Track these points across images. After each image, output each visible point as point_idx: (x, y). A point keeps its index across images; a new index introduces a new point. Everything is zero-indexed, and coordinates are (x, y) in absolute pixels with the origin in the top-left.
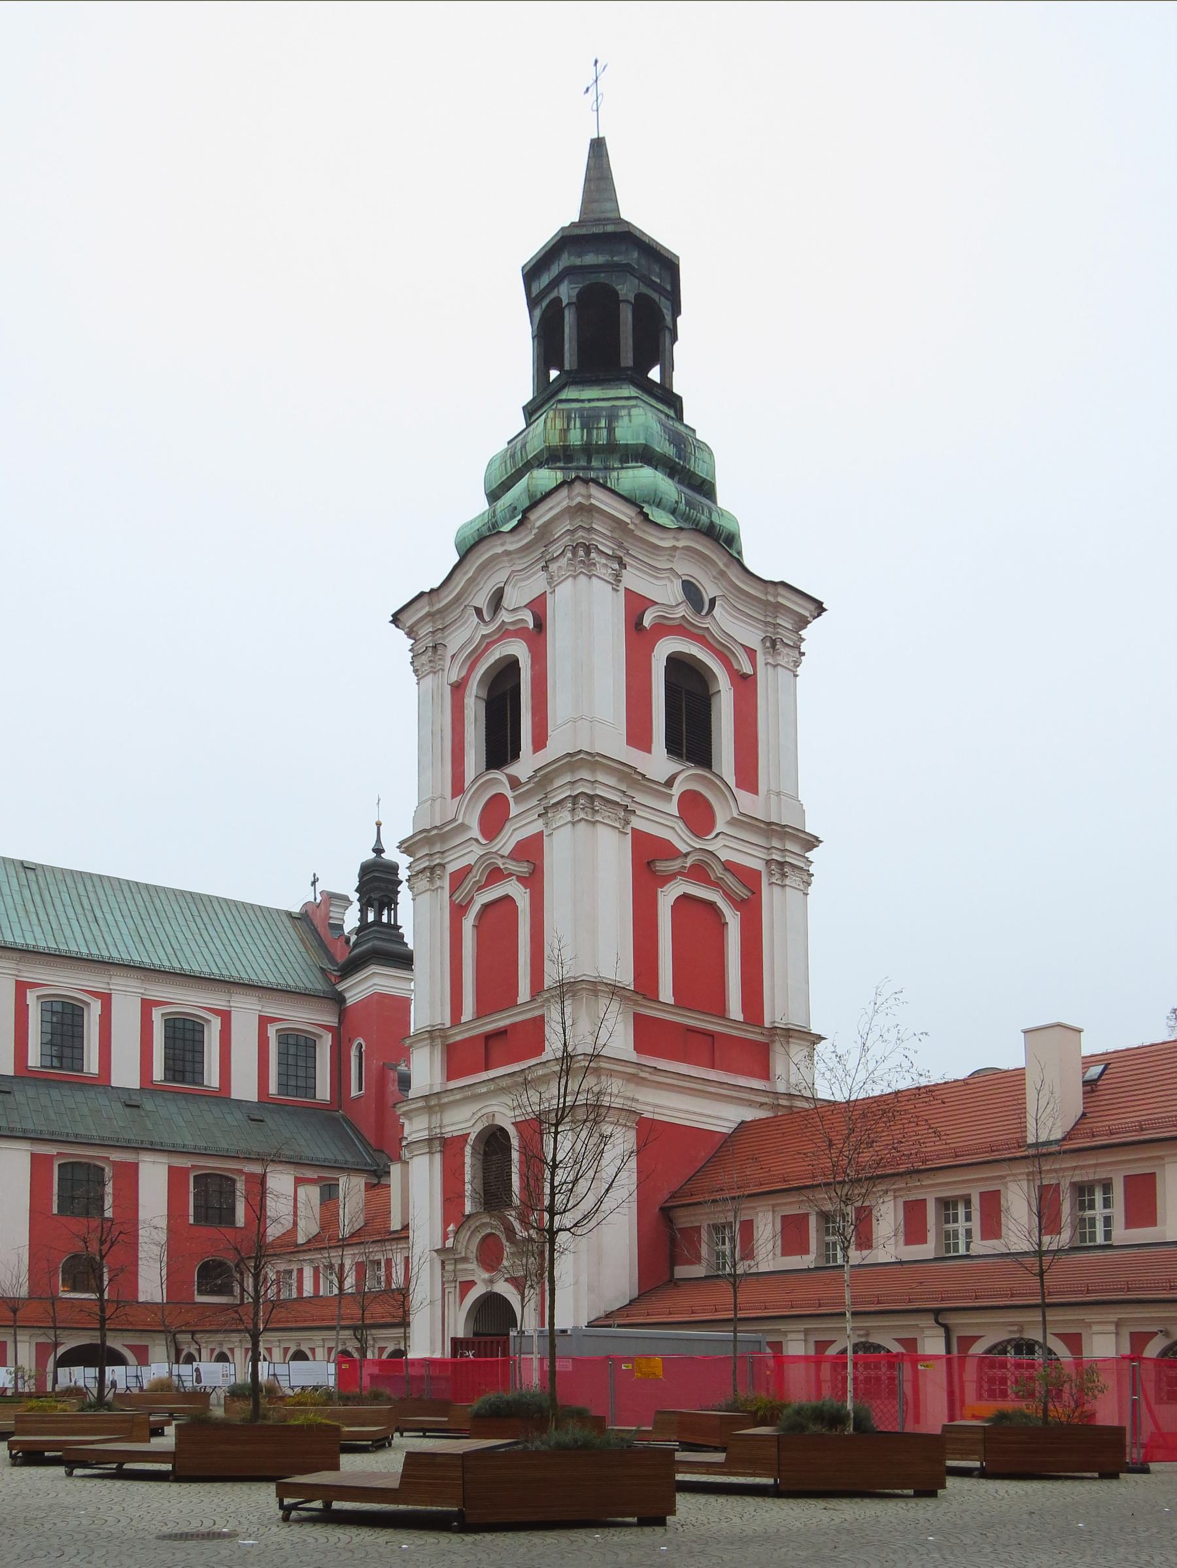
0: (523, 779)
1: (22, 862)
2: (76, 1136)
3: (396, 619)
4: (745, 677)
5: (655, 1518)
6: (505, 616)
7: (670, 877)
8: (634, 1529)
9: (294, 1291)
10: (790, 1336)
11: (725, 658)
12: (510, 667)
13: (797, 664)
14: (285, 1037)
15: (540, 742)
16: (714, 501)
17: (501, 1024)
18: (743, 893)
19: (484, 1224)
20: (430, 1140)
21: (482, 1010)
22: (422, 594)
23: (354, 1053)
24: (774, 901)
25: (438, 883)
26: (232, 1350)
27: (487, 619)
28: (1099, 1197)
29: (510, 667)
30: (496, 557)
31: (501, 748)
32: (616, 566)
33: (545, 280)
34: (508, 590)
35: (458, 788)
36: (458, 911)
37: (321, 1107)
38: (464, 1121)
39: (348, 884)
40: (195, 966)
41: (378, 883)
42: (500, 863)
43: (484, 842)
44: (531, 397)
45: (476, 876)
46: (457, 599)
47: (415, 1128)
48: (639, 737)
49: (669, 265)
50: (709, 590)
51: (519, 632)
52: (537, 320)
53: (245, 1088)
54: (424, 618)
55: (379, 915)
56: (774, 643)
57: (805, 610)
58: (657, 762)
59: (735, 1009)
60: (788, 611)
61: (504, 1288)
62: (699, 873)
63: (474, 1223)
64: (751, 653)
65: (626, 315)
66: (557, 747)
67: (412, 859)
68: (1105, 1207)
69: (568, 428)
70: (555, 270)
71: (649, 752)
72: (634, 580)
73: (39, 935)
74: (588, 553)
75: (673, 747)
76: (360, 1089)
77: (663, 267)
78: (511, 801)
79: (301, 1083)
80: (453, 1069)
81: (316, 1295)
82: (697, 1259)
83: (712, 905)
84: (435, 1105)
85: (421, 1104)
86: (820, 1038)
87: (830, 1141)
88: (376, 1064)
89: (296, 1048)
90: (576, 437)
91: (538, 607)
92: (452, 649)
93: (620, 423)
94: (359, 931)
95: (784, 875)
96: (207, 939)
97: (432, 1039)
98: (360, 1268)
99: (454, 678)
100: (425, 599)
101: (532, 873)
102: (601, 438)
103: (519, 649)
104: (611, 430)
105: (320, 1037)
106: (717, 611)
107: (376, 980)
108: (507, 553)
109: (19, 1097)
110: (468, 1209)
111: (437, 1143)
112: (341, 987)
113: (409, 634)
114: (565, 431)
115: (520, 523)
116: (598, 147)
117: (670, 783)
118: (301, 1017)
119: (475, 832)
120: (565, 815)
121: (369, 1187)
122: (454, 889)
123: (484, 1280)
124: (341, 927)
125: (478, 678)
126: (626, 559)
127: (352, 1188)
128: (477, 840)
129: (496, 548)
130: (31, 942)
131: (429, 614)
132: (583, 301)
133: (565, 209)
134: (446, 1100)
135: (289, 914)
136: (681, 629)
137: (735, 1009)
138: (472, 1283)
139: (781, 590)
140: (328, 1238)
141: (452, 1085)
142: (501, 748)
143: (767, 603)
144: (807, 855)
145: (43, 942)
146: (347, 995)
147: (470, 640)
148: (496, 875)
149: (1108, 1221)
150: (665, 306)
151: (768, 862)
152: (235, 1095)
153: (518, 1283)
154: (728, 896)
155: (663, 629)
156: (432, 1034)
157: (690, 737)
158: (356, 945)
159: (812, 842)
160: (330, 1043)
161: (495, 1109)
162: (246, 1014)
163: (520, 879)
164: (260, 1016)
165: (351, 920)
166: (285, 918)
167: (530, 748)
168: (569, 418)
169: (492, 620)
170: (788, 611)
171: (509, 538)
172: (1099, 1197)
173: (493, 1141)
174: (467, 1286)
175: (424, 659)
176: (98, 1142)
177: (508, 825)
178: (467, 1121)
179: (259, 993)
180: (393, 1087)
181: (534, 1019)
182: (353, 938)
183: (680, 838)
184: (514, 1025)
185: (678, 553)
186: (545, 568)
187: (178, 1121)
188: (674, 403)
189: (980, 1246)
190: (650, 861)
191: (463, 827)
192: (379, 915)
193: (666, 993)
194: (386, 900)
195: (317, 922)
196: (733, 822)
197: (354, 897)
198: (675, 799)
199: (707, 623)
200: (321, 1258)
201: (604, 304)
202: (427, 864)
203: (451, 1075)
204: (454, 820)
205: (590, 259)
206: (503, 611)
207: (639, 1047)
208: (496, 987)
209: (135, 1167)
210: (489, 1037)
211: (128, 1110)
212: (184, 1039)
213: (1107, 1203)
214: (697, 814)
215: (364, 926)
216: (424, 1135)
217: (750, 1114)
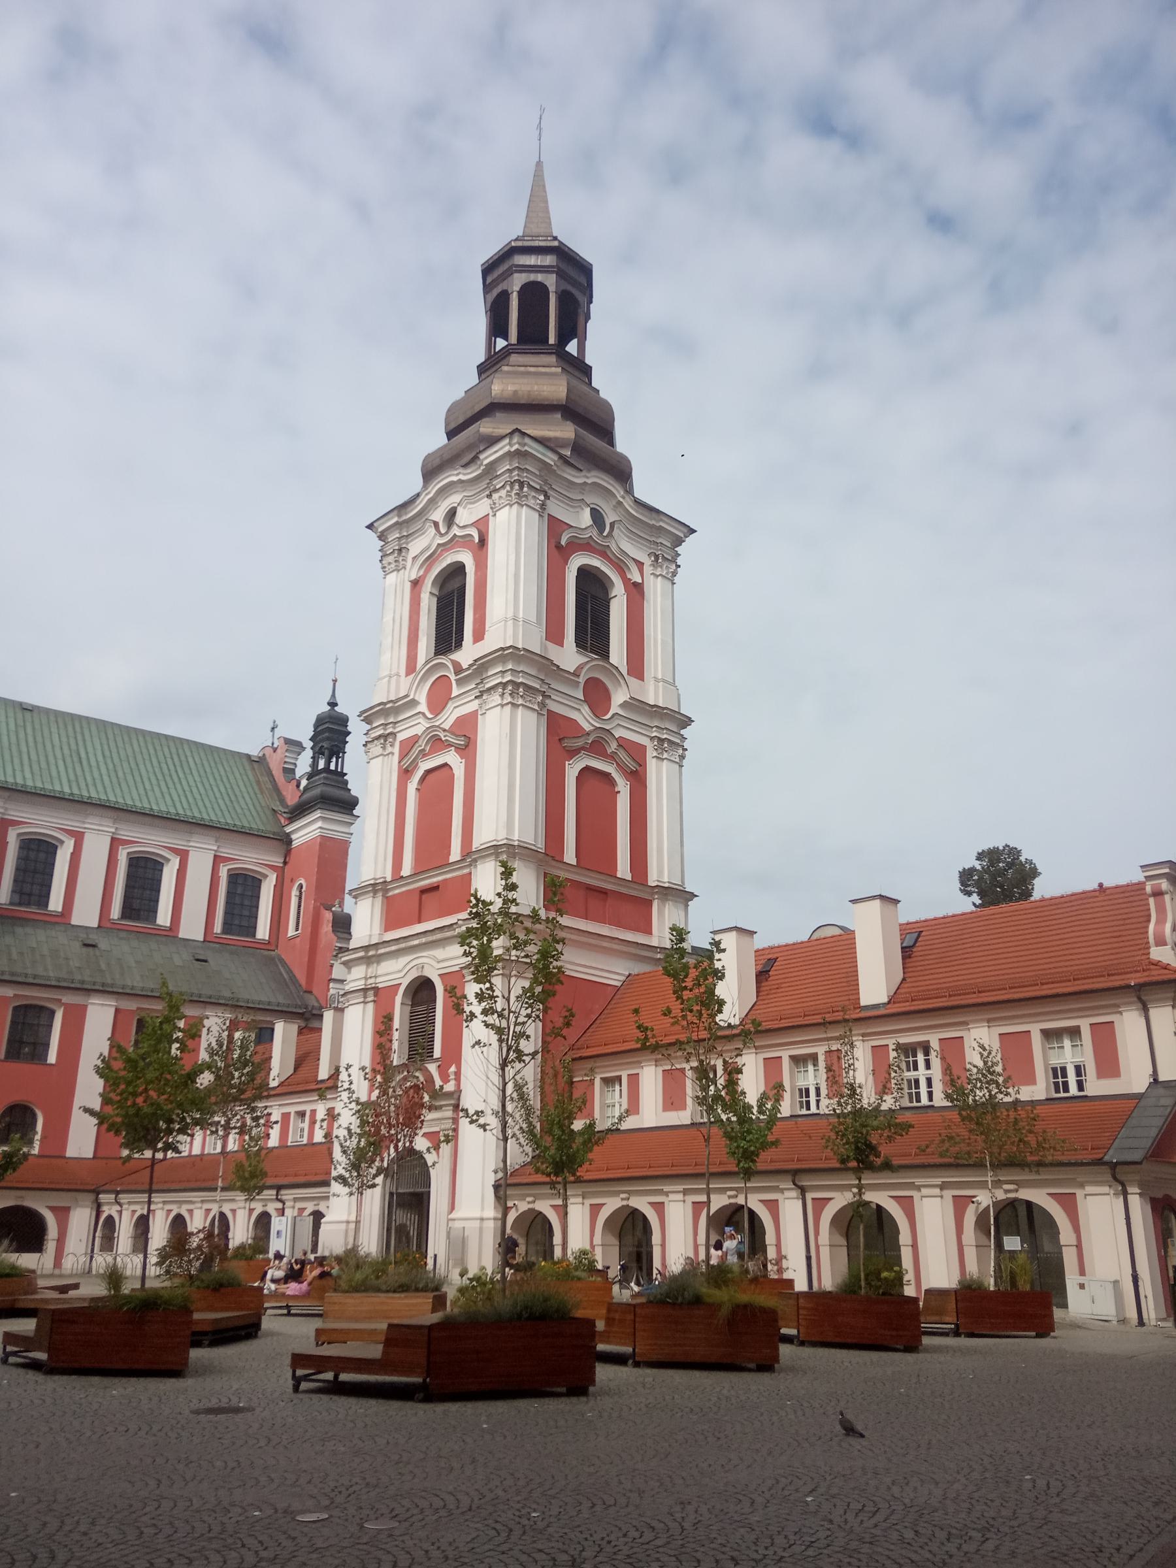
0: (465, 666)
1: (21, 704)
2: (35, 977)
4: (635, 584)
5: (580, 1387)
6: (455, 531)
8: (563, 1399)
10: (672, 1197)
11: (621, 569)
12: (458, 570)
14: (234, 877)
15: (479, 636)
16: (611, 443)
17: (435, 880)
18: (632, 766)
20: (365, 990)
23: (295, 892)
24: (658, 773)
25: (389, 749)
27: (443, 531)
29: (458, 570)
30: (452, 483)
31: (448, 636)
32: (542, 498)
34: (460, 510)
35: (411, 668)
36: (406, 773)
38: (396, 972)
39: (304, 733)
40: (160, 806)
41: (331, 733)
42: (442, 735)
43: (430, 716)
44: (483, 360)
45: (422, 743)
48: (554, 634)
49: (585, 270)
50: (610, 517)
52: (489, 305)
54: (395, 528)
55: (328, 763)
56: (657, 557)
58: (569, 656)
60: (666, 535)
64: (640, 565)
66: (494, 639)
67: (369, 727)
71: (562, 646)
72: (557, 509)
73: (28, 775)
74: (521, 487)
75: (581, 643)
76: (297, 929)
78: (454, 683)
79: (245, 923)
80: (390, 922)
83: (607, 775)
84: (373, 956)
86: (693, 896)
91: (482, 525)
92: (412, 554)
94: (310, 776)
99: (413, 577)
101: (467, 746)
106: (616, 532)
108: (461, 481)
111: (371, 993)
112: (288, 830)
117: (576, 674)
118: (250, 858)
119: (423, 707)
120: (495, 699)
121: (301, 1032)
124: (293, 771)
125: (433, 577)
126: (550, 492)
128: (424, 714)
130: (20, 781)
131: (397, 523)
135: (248, 756)
136: (587, 546)
142: (448, 636)
144: (682, 732)
146: (293, 837)
147: (427, 548)
148: (437, 743)
152: (182, 934)
154: (621, 767)
155: (577, 545)
156: (376, 888)
157: (593, 633)
158: (306, 789)
159: (686, 722)
163: (458, 749)
166: (245, 760)
169: (447, 533)
170: (666, 535)
175: (391, 559)
176: (53, 983)
177: (451, 705)
178: (400, 971)
179: (217, 833)
182: (304, 783)
183: (584, 718)
185: (587, 488)
186: (489, 496)
187: (130, 959)
188: (585, 371)
192: (328, 763)
193: (570, 857)
194: (335, 749)
197: (308, 744)
202: (381, 732)
203: (389, 925)
204: (406, 696)
206: (455, 527)
207: (549, 903)
209: (84, 1008)
210: (424, 891)
211: (85, 950)
212: (143, 876)
213: (928, 1065)
214: (597, 695)
216: (360, 984)
217: (637, 968)
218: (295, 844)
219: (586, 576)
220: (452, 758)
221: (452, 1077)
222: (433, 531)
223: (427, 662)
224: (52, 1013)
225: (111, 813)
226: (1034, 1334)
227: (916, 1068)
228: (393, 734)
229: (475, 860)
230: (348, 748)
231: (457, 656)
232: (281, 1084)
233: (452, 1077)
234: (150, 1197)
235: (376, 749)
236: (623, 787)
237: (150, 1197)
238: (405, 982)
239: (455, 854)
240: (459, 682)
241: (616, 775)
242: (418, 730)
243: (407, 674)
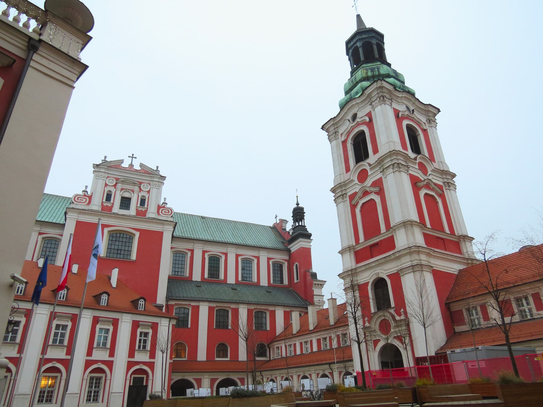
3: (323, 128)
6: (358, 120)
7: (420, 188)
9: (328, 345)
13: (436, 126)
14: (274, 264)
15: (376, 151)
17: (376, 241)
18: (440, 192)
19: (381, 316)
21: (367, 237)
22: (331, 119)
23: (295, 268)
26: (276, 378)
28: (474, 312)
29: (362, 133)
33: (352, 43)
34: (358, 113)
35: (348, 170)
36: (353, 207)
37: (285, 287)
40: (250, 242)
46: (341, 119)
48: (404, 147)
49: (381, 36)
50: (412, 108)
51: (364, 123)
53: (264, 282)
54: (330, 127)
55: (299, 223)
57: (435, 111)
59: (447, 230)
60: (431, 112)
62: (427, 186)
63: (376, 317)
65: (375, 47)
66: (383, 150)
70: (355, 40)
72: (395, 105)
74: (383, 98)
76: (297, 279)
77: (380, 37)
81: (286, 356)
87: (506, 270)
88: (303, 270)
89: (278, 267)
90: (370, 74)
91: (369, 115)
92: (341, 132)
94: (293, 229)
95: (449, 186)
97: (350, 250)
98: (319, 341)
99: (343, 139)
100: (332, 120)
101: (380, 190)
102: (377, 73)
103: (365, 128)
104: (379, 71)
105: (284, 263)
107: (301, 243)
108: (357, 103)
109: (203, 288)
110: (373, 311)
112: (289, 247)
113: (326, 131)
114: (367, 73)
115: (362, 94)
116: (358, 16)
119: (357, 182)
120: (391, 170)
122: (351, 201)
123: (385, 339)
124: (285, 229)
127: (295, 316)
129: (354, 102)
131: (333, 124)
132: (363, 46)
133: (353, 29)
135: (270, 227)
136: (407, 118)
137: (447, 230)
138: (379, 340)
139: (429, 107)
141: (359, 265)
143: (425, 110)
145: (210, 238)
146: (291, 249)
148: (366, 193)
150: (382, 44)
151: (444, 183)
153: (399, 338)
154: (436, 194)
158: (293, 233)
159: (454, 176)
161: (379, 271)
162: (264, 256)
163: (375, 193)
165: (289, 227)
167: (373, 154)
170: (431, 112)
171: (357, 99)
172: (474, 312)
173: (380, 283)
174: (376, 342)
177: (369, 179)
180: (309, 278)
181: (389, 238)
184: (381, 241)
186: (371, 104)
190: (415, 182)
191: (352, 181)
192: (299, 223)
195: (278, 228)
196: (433, 171)
199: (413, 116)
200: (303, 339)
201: (366, 47)
203: (357, 262)
205: (364, 36)
208: (371, 228)
213: (528, 304)
215: (294, 228)
218: (292, 251)
219: (409, 127)
220: (373, 196)
221: (402, 313)
222: (348, 122)
223: (355, 167)
224: (228, 311)
225: (234, 246)
226: (131, 384)
228: (346, 194)
229: (395, 230)
230: (305, 217)
231: (368, 161)
232: (297, 333)
233: (402, 313)
235: (340, 200)
236: (439, 200)
240: (371, 169)
241: (436, 196)
242: (357, 190)
243: (347, 173)
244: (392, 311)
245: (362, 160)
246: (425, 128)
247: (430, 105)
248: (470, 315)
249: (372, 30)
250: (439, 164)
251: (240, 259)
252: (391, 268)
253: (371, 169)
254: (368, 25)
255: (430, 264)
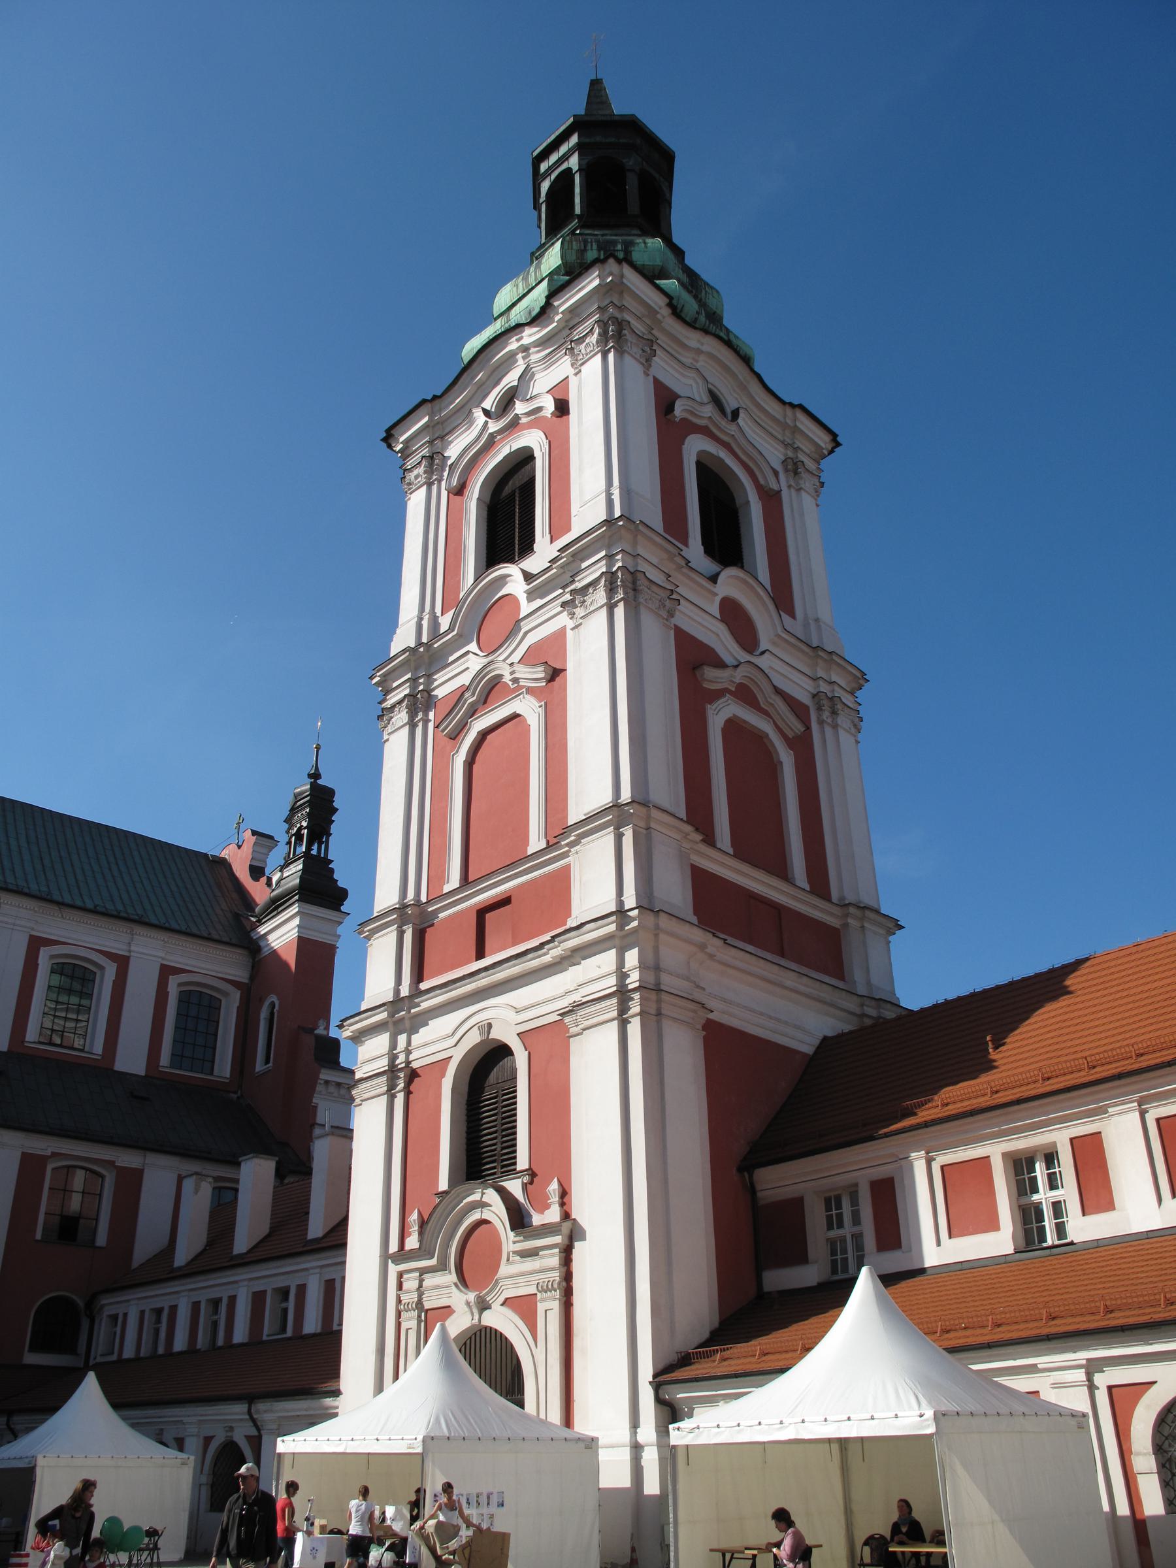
7: (718, 694)
12: (525, 458)
14: (186, 998)
22: (424, 402)
29: (525, 458)
38: (443, 1040)
47: (369, 1056)
49: (666, 158)
50: (731, 403)
61: (501, 1320)
62: (744, 694)
68: (854, 1224)
69: (585, 250)
72: (663, 368)
75: (709, 550)
76: (267, 1061)
82: (800, 1257)
85: (382, 1016)
89: (198, 1008)
93: (636, 248)
96: (116, 873)
100: (426, 408)
134: (425, 1005)
138: (447, 1311)
139: (800, 415)
140: (217, 1254)
143: (784, 426)
149: (1058, 1208)
160: (237, 1004)
164: (162, 966)
168: (585, 242)
189: (1083, 1228)
198: (718, 600)
210: (482, 913)
227: (840, 1225)
230: (334, 829)
234: (421, 1281)
237: (421, 1281)
238: (458, 1055)
239: (536, 843)
244: (514, 1187)
245: (511, 560)
246: (774, 485)
247: (801, 407)
248: (834, 1222)
249: (632, 125)
250: (806, 625)
251: (45, 959)
252: (542, 998)
253: (531, 595)
254: (620, 107)
255: (698, 995)
